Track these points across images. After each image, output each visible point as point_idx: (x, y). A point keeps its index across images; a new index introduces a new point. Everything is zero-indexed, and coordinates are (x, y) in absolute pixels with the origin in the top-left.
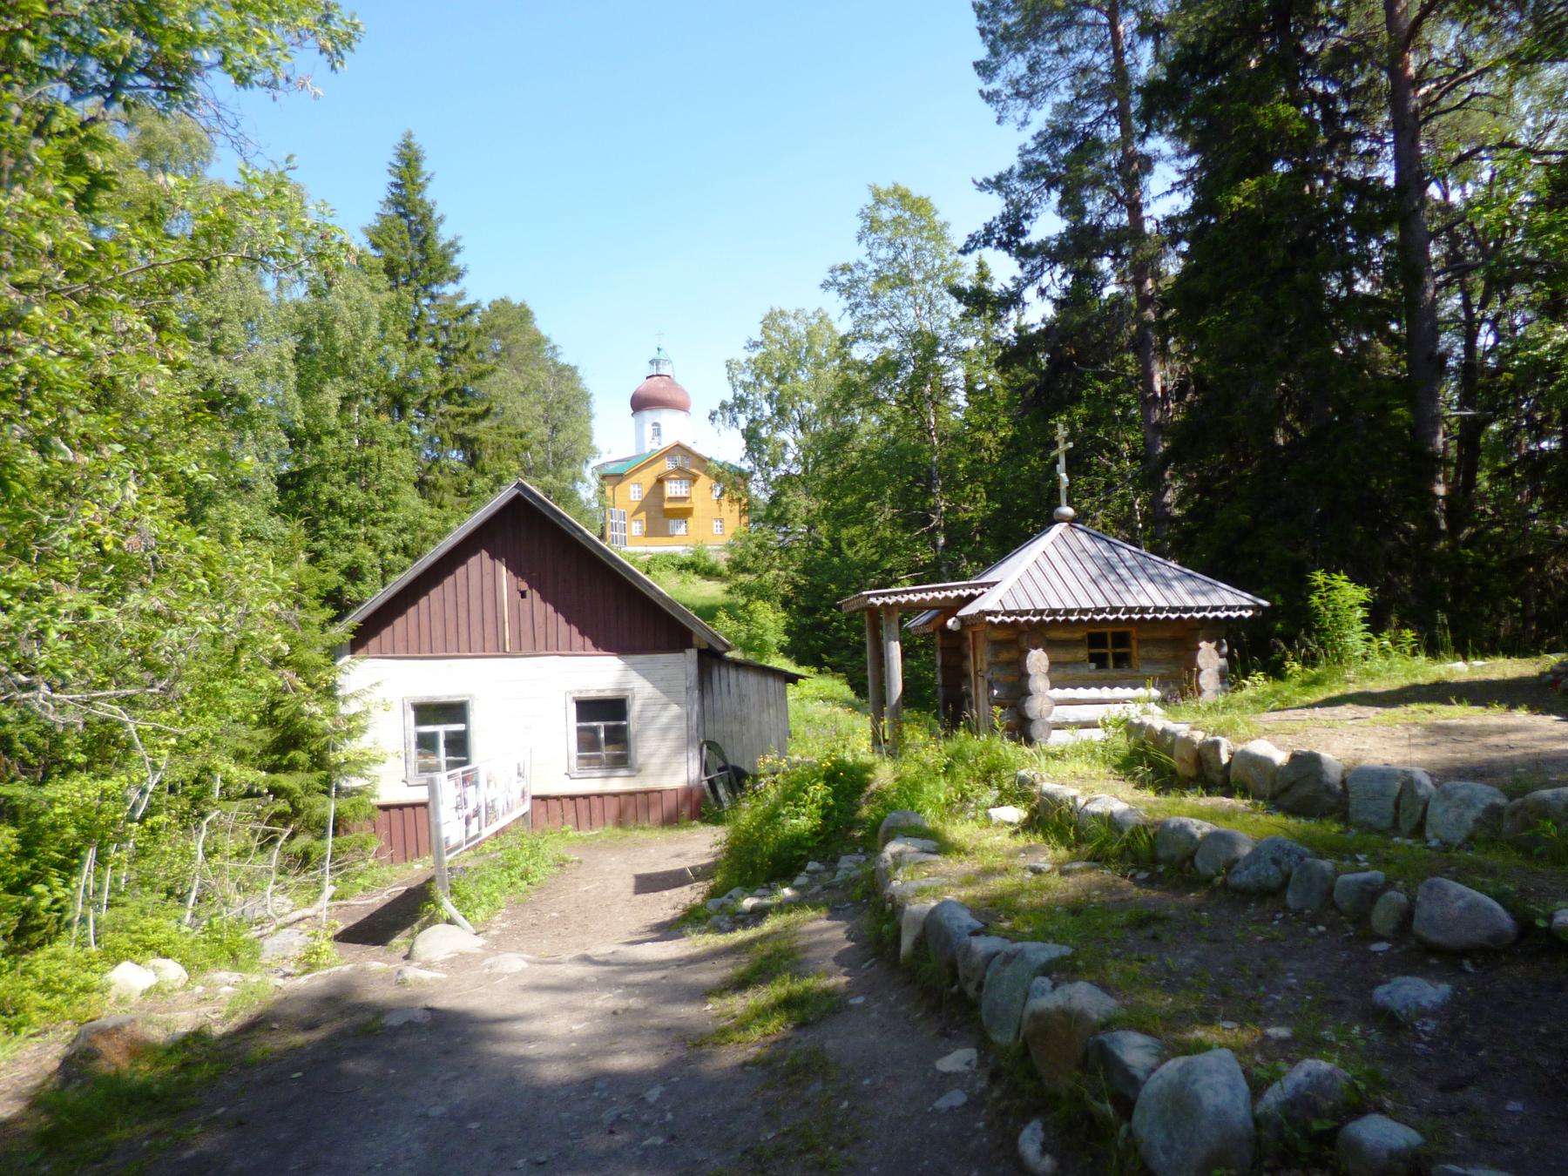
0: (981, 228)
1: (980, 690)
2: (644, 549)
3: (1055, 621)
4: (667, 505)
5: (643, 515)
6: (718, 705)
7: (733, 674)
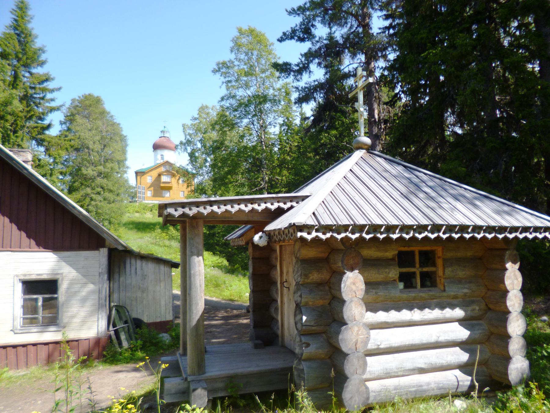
0: (290, 30)
1: (286, 300)
2: (152, 202)
3: (375, 239)
4: (162, 185)
5: (152, 188)
6: (128, 281)
7: (139, 263)
